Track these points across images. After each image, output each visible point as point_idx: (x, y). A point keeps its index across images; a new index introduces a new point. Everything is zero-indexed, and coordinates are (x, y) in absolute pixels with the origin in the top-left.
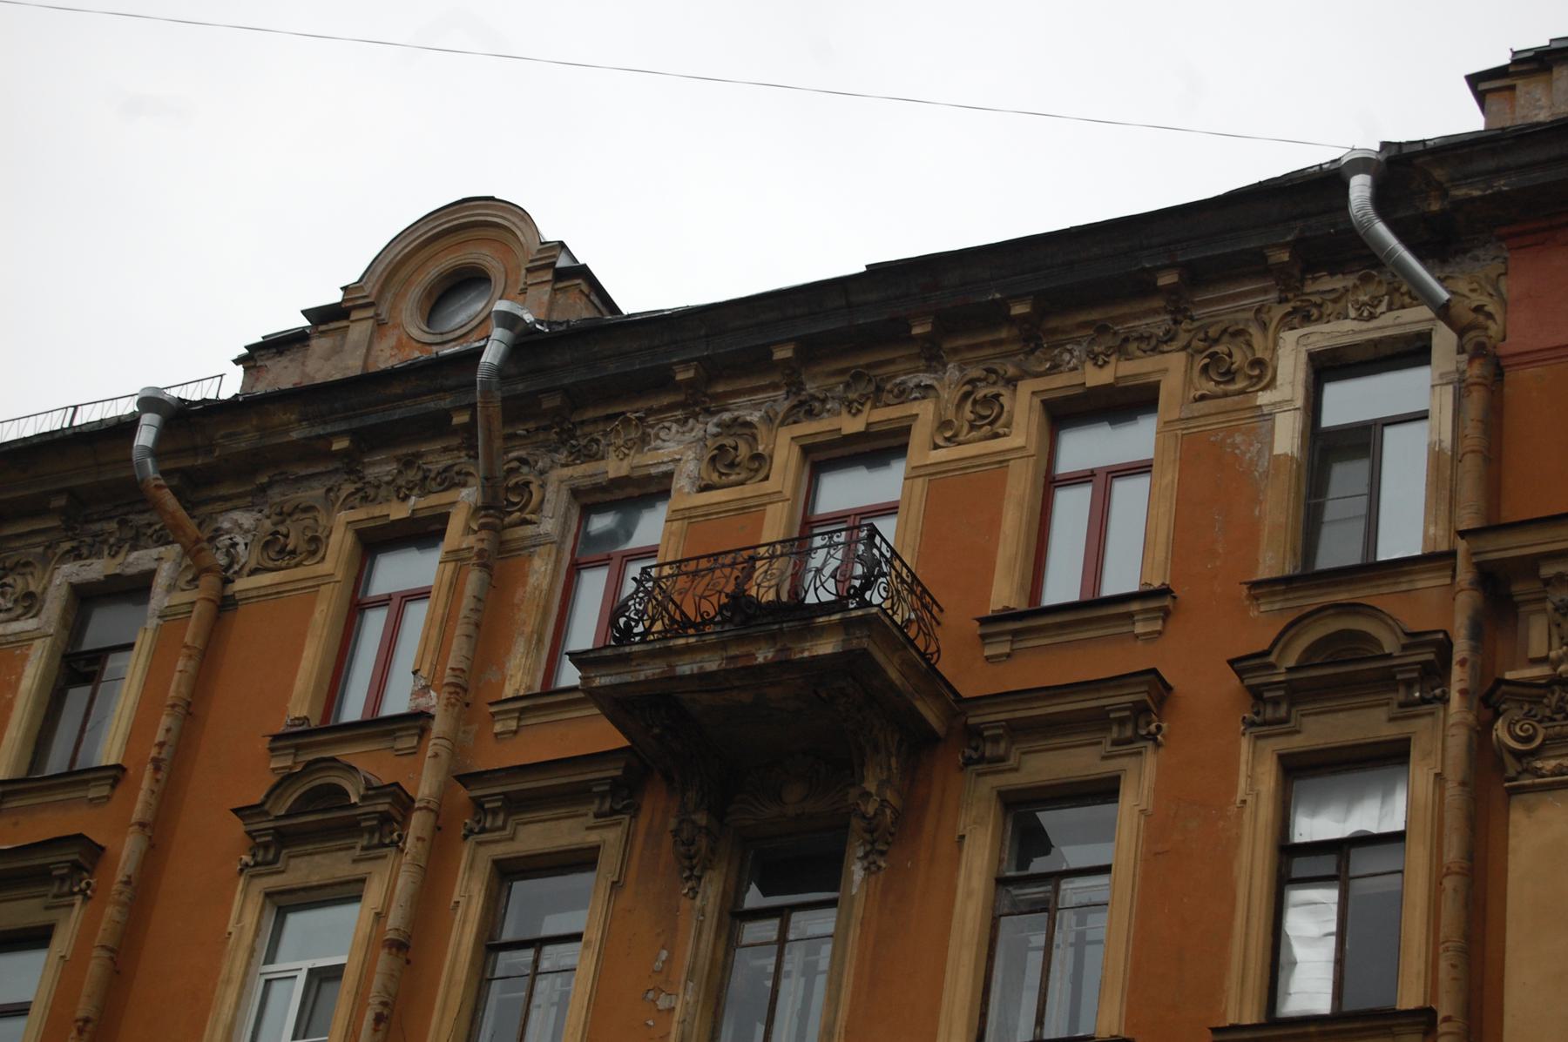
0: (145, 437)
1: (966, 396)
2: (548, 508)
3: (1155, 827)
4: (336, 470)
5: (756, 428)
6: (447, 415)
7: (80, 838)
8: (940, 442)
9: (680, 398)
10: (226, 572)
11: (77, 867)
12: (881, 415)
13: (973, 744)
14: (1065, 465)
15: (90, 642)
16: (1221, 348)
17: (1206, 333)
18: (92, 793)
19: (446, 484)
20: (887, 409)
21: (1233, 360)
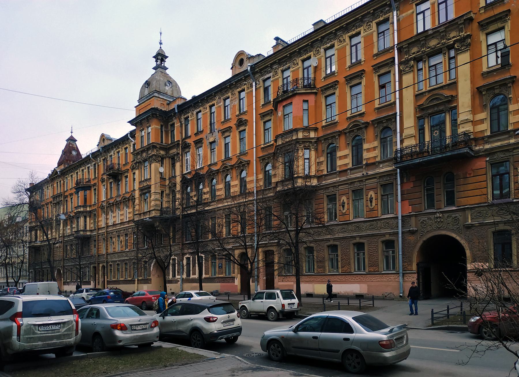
0: (48, 178)
2: (279, 73)
3: (339, 96)
6: (192, 105)
7: (230, 126)
9: (371, 15)
10: (71, 175)
11: (271, 112)
15: (266, 86)
18: (390, 51)
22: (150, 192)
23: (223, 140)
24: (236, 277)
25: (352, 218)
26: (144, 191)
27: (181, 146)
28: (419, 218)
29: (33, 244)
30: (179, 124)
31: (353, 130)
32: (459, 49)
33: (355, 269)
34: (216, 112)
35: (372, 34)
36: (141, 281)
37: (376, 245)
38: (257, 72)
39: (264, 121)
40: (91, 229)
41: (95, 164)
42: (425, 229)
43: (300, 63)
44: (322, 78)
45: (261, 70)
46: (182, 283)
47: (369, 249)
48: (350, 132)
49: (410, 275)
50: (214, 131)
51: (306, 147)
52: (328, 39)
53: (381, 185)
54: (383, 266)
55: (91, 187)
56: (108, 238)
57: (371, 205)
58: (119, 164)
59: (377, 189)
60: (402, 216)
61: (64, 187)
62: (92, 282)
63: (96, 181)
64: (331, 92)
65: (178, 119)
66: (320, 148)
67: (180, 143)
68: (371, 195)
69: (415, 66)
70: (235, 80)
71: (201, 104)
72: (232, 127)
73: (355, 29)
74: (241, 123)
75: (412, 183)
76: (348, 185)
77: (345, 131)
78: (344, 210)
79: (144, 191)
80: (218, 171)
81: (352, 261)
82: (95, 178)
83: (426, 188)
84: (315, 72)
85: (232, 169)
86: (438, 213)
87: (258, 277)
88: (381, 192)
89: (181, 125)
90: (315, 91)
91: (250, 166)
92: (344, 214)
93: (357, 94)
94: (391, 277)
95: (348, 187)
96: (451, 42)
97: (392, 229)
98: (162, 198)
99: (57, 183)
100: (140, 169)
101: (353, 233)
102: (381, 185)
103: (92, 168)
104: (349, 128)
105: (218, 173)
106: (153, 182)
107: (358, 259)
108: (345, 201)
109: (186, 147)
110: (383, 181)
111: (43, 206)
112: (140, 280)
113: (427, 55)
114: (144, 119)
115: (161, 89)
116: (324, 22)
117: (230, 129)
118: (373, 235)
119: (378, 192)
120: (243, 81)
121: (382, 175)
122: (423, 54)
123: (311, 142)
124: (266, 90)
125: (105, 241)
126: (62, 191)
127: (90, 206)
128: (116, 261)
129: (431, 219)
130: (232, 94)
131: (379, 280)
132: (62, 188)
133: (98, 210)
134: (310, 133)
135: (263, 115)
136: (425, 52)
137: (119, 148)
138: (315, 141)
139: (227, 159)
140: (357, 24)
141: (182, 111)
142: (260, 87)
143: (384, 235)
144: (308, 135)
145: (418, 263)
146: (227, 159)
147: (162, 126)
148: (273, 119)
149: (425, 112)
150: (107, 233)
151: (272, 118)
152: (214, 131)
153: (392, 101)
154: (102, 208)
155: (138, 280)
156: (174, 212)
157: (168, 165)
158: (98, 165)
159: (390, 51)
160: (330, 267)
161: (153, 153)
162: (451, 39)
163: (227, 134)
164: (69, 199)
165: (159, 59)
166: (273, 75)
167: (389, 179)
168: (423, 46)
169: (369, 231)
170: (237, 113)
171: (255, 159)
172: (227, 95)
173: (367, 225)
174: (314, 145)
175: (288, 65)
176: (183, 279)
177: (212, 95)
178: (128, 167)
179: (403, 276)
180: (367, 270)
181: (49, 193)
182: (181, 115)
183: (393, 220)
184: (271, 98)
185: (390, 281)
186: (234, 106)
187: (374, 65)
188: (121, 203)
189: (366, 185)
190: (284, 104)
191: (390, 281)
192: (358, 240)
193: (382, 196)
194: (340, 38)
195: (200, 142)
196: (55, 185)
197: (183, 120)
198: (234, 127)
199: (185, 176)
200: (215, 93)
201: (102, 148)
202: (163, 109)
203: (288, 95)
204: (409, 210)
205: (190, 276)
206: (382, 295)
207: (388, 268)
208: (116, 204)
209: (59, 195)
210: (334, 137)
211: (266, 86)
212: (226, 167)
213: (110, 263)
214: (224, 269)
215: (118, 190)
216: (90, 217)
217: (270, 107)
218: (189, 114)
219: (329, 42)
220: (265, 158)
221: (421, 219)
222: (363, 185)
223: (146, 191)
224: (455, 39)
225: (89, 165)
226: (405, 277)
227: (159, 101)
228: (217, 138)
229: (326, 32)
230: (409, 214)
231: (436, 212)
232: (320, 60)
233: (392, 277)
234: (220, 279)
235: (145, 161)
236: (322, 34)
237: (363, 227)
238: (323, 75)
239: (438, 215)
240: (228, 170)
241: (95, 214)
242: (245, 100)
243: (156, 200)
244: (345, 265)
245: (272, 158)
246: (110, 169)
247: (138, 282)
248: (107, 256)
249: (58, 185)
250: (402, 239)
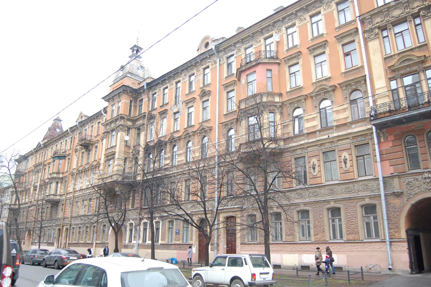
2: (242, 51)
3: (303, 65)
11: (235, 83)
14: (267, 44)
16: (301, 18)
18: (352, 24)
22: (114, 158)
23: (187, 110)
24: (193, 244)
25: (325, 181)
26: (109, 158)
27: (146, 117)
28: (403, 180)
29: (12, 206)
30: (147, 99)
31: (320, 93)
32: (425, 15)
33: (330, 237)
34: (181, 87)
35: (332, 12)
36: (99, 245)
37: (355, 209)
38: (221, 51)
39: (227, 91)
40: (61, 194)
41: (72, 138)
42: (412, 191)
43: (262, 41)
44: (284, 51)
45: (225, 49)
46: (138, 249)
47: (347, 214)
48: (316, 96)
49: (398, 244)
50: (179, 103)
51: (271, 110)
52: (289, 19)
53: (355, 146)
54: (365, 233)
55: (66, 157)
56: (74, 201)
57: (346, 167)
58: (91, 136)
59: (351, 150)
60: (383, 178)
61: (44, 157)
62: (55, 243)
63: (70, 152)
64: (295, 61)
65: (146, 95)
66: (285, 110)
67: (147, 115)
68: (345, 156)
69: (380, 34)
70: (200, 58)
71: (168, 81)
72: (195, 98)
73: (315, 9)
74: (204, 93)
75: (391, 142)
76: (317, 147)
77: (311, 95)
78: (314, 172)
79: (109, 158)
80: (180, 138)
81: (326, 228)
82: (71, 149)
83: (407, 148)
84: (277, 46)
85: (194, 135)
86: (426, 173)
87: (218, 245)
88: (356, 153)
89: (149, 99)
90: (278, 61)
91: (213, 132)
92: (315, 177)
93: (321, 62)
94: (375, 246)
95: (318, 149)
96: (416, 10)
97: (372, 192)
98: (124, 165)
99: (40, 154)
100: (108, 138)
101: (326, 197)
102: (355, 146)
103: (69, 141)
104: (316, 92)
105: (180, 140)
106: (117, 150)
107: (334, 226)
108: (316, 162)
109: (151, 117)
110: (357, 142)
111: (26, 173)
112: (98, 243)
113: (391, 23)
114: (116, 95)
115: (134, 72)
116: (283, 7)
117: (194, 100)
118: (350, 199)
119: (352, 153)
120: (207, 59)
121: (356, 136)
122: (387, 23)
123: (276, 106)
124: (229, 65)
125: (71, 206)
126: (43, 161)
127: (63, 173)
128: (78, 224)
129: (417, 180)
130: (197, 71)
131: (361, 249)
132: (43, 158)
133: (69, 177)
134: (274, 98)
135: (226, 86)
136: (389, 21)
137: (93, 123)
138: (280, 105)
139: (190, 126)
140: (316, 6)
141: (151, 88)
142: (224, 63)
143: (363, 198)
144: (272, 99)
145: (407, 230)
146: (190, 126)
147: (131, 101)
148: (237, 89)
149: (396, 73)
150: (74, 198)
151: (235, 88)
152: (179, 103)
153: (359, 65)
154: (72, 174)
155: (96, 244)
156: (135, 177)
157: (133, 135)
158: (74, 138)
159: (352, 24)
160: (301, 235)
161: (120, 123)
162: (414, 8)
163: (190, 105)
164: (47, 168)
165: (135, 50)
166: (236, 52)
167: (363, 139)
168: (386, 16)
169: (345, 195)
170: (201, 85)
171: (217, 125)
172: (192, 72)
173: (342, 188)
174: (278, 109)
175: (251, 43)
176: (139, 244)
177: (178, 73)
178: (99, 138)
179: (391, 245)
180: (345, 238)
181: (31, 163)
182: (149, 92)
183: (372, 182)
184: (234, 71)
185: (374, 251)
186: (199, 80)
187: (338, 36)
188: (89, 170)
189: (337, 146)
190: (248, 72)
191: (374, 251)
192: (332, 204)
193: (357, 157)
194: (301, 18)
195: (164, 113)
196: (38, 156)
197: (151, 96)
198: (198, 98)
199: (148, 143)
200: (182, 71)
201: (79, 123)
202: (134, 88)
203: (251, 65)
204: (390, 170)
205: (145, 241)
206: (366, 267)
207: (369, 235)
208: (84, 171)
209: (40, 164)
210: (300, 100)
211: (229, 62)
212: (188, 133)
213: (73, 226)
214: (181, 235)
215: (88, 158)
216: (62, 183)
217: (234, 78)
218: (157, 91)
219: (290, 22)
220: (227, 124)
221: (405, 180)
222: (335, 146)
223: (111, 157)
224: (420, 7)
225: (67, 138)
226: (392, 246)
227: (131, 81)
228: (181, 108)
229: (287, 13)
230: (391, 175)
231: (424, 172)
232: (282, 37)
233: (377, 246)
234: (177, 246)
235: (113, 131)
236: (283, 15)
237: (338, 191)
238: (286, 48)
239: (426, 175)
240: (189, 136)
241: (66, 181)
242: (209, 76)
243: (119, 165)
244: (318, 232)
245: (235, 123)
246: (83, 140)
247: (96, 245)
248: (71, 220)
249: (40, 156)
250: (386, 202)
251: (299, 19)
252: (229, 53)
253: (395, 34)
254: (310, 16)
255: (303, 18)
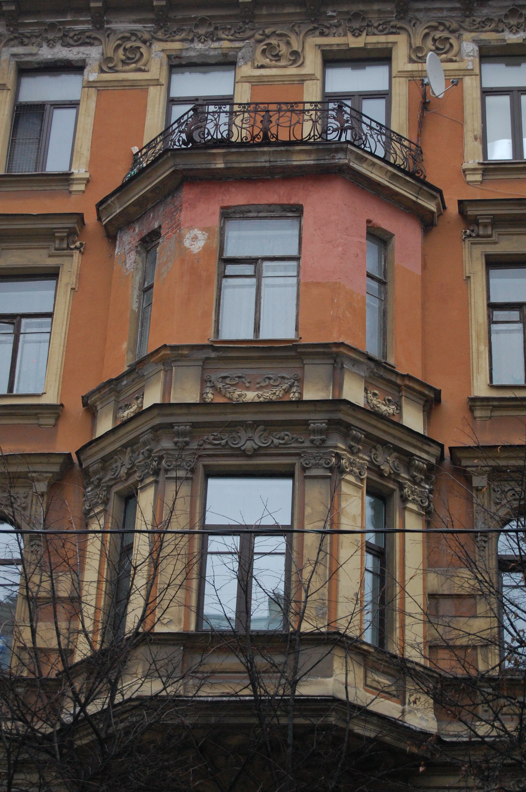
1: (119, 46)
4: (235, 16)
5: (289, 37)
8: (105, 68)
11: (72, 233)
12: (382, 39)
13: (471, 228)
17: (264, 31)
19: (80, 42)
20: (373, 37)
21: (280, 49)
203: (281, 161)
251: (261, 47)
252: (51, 44)
253: (492, 307)
254: (18, 64)
255: (283, 49)
